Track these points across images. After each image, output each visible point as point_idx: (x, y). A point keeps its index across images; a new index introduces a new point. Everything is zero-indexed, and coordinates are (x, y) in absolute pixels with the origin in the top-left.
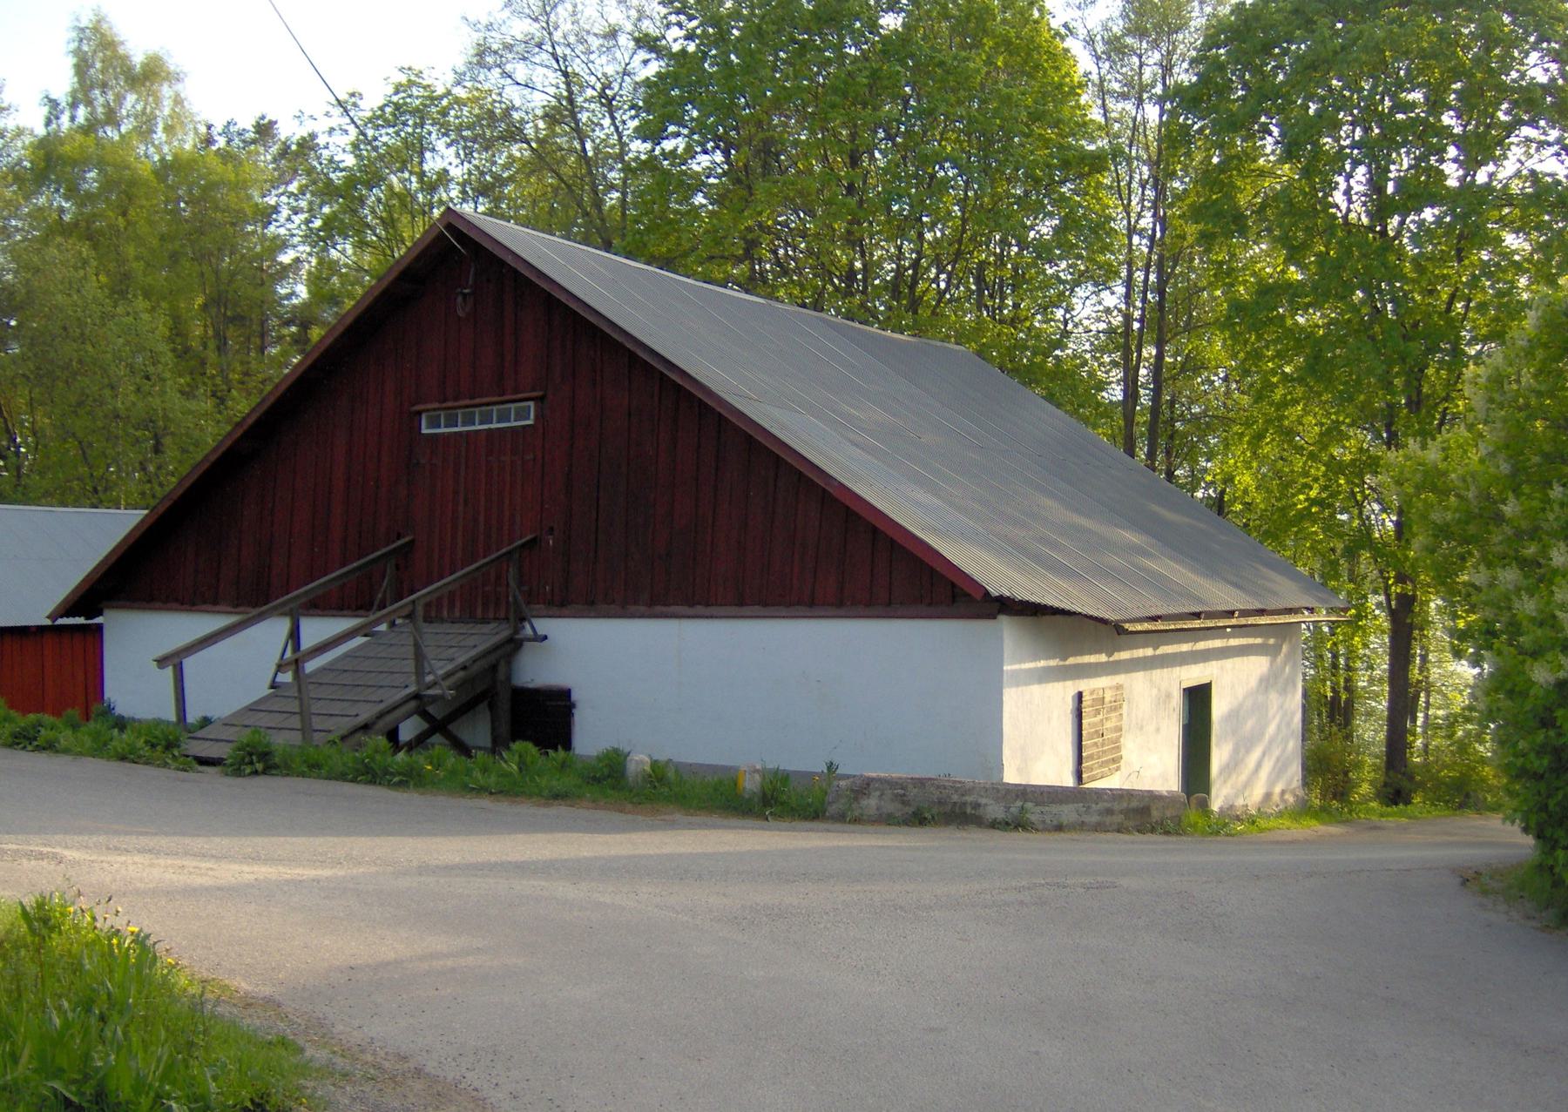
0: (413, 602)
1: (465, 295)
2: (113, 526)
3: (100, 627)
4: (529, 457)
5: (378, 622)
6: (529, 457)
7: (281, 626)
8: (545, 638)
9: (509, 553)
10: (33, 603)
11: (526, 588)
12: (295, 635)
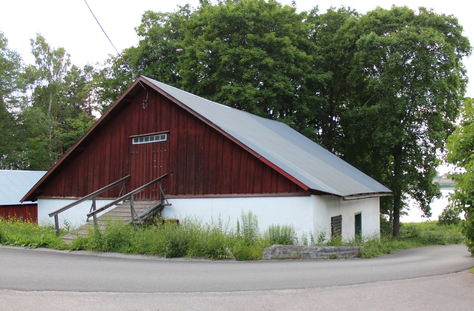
0: (130, 194)
1: (145, 102)
2: (37, 176)
3: (36, 204)
4: (165, 150)
5: (120, 201)
6: (165, 150)
7: (91, 202)
8: (171, 205)
9: (160, 179)
10: (15, 197)
11: (165, 190)
12: (94, 205)
